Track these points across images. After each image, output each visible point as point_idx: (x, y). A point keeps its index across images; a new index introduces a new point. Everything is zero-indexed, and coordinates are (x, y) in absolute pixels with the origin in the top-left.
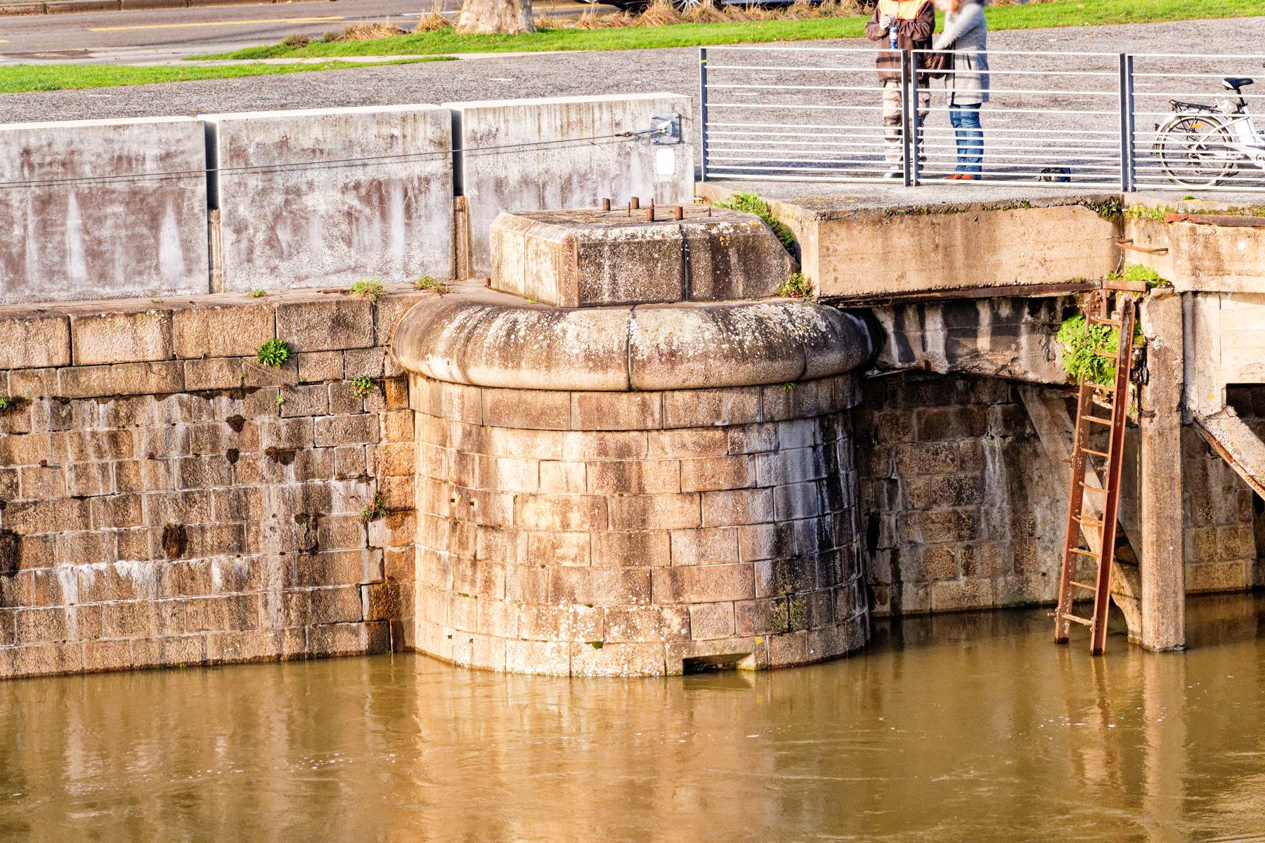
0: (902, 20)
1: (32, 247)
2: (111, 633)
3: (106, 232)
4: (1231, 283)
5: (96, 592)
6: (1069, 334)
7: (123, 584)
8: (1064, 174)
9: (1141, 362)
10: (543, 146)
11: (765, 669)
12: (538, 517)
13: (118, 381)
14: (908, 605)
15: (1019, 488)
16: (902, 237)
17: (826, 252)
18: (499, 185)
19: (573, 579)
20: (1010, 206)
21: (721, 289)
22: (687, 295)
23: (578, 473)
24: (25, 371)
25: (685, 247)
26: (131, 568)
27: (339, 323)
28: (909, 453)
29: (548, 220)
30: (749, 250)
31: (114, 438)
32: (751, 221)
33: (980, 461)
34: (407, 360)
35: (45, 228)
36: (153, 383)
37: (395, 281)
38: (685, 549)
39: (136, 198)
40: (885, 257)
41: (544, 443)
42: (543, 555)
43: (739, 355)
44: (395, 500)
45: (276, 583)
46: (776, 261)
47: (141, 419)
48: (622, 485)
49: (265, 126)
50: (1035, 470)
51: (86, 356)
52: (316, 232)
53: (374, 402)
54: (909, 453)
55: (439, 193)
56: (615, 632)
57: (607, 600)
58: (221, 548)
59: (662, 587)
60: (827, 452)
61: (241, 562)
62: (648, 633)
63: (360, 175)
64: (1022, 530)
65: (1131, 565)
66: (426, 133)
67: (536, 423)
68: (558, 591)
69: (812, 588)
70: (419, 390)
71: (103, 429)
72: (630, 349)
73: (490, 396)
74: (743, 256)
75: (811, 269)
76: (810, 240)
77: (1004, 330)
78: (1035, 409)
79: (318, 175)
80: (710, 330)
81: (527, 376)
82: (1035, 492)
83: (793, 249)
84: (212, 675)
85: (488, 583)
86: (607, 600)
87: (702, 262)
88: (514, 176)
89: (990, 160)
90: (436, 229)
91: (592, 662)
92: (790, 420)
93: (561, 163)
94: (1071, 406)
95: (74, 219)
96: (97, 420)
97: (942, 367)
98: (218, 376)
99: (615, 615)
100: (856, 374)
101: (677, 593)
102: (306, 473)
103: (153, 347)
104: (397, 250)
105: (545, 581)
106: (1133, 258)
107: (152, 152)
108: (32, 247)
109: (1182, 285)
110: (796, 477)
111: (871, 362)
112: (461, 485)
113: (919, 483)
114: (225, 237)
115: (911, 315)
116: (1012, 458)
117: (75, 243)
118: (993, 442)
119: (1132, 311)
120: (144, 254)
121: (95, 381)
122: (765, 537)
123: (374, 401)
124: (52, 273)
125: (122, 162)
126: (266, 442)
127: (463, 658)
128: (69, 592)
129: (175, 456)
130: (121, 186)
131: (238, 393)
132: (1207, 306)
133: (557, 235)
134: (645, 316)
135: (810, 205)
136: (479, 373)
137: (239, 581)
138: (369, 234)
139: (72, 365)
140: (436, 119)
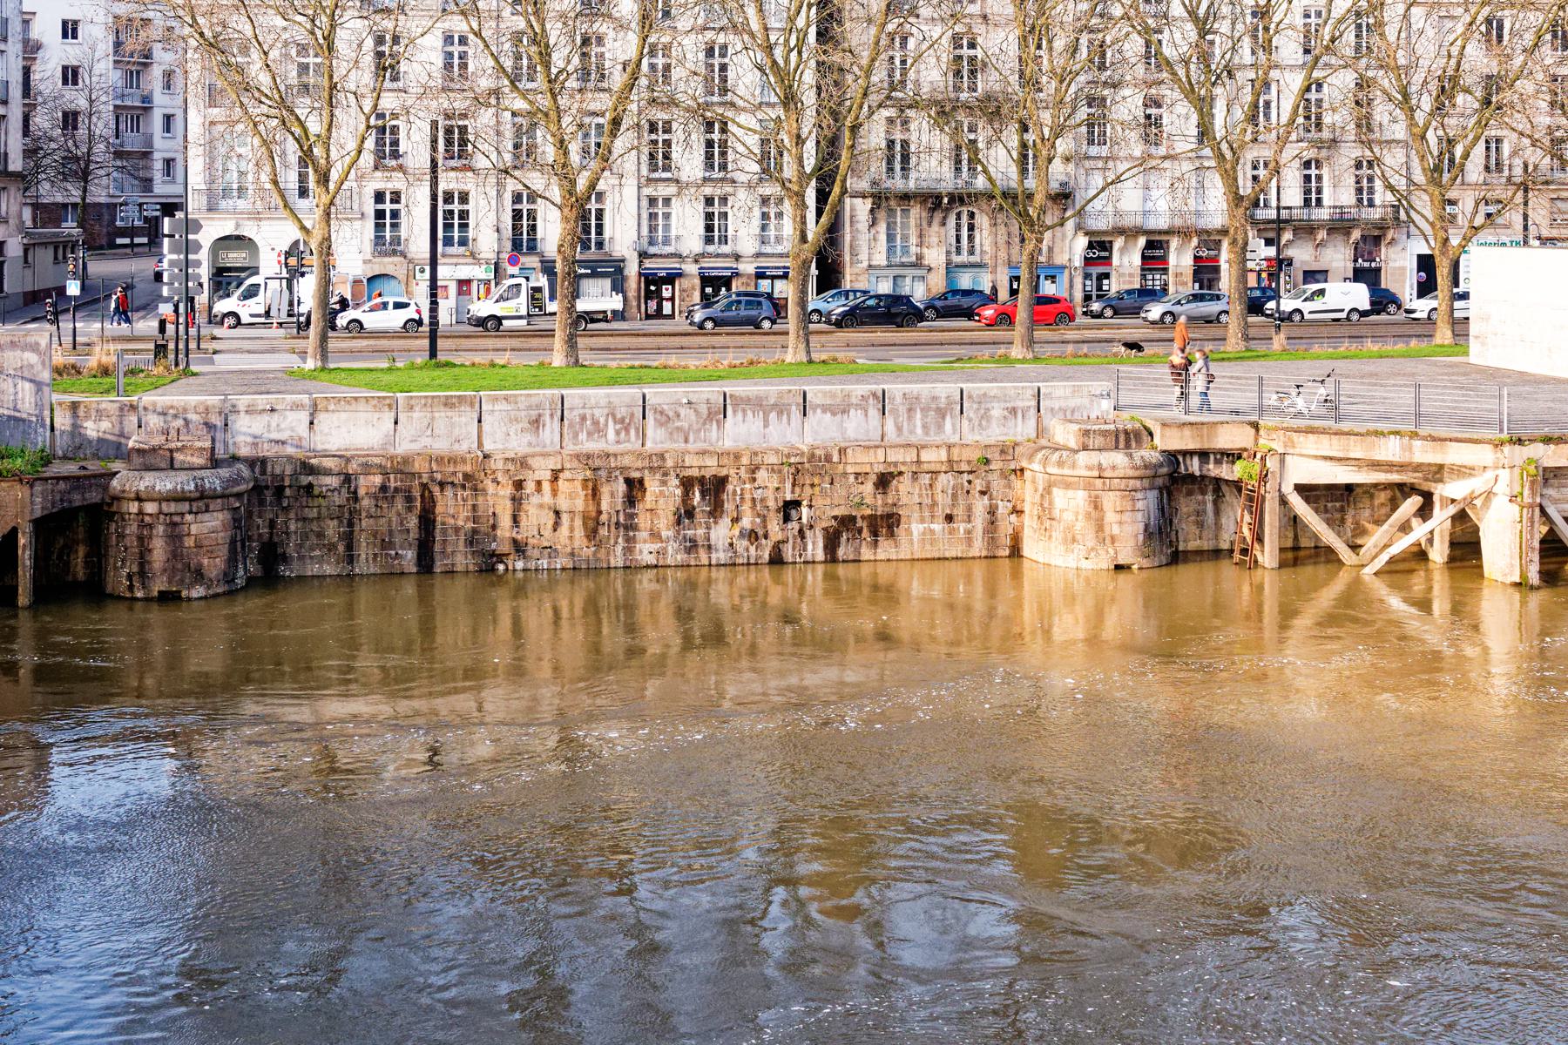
1: (905, 424)
2: (928, 547)
4: (1297, 451)
5: (924, 534)
6: (1239, 465)
7: (932, 532)
8: (1237, 413)
9: (1266, 475)
10: (1066, 398)
11: (1140, 569)
12: (1068, 517)
13: (933, 467)
14: (1181, 548)
15: (1217, 512)
16: (1187, 432)
17: (1162, 436)
18: (1052, 409)
19: (1078, 537)
20: (1222, 423)
21: (1128, 446)
22: (1117, 448)
23: (1082, 503)
24: (904, 463)
25: (1117, 433)
27: (1002, 452)
29: (1071, 421)
30: (1137, 435)
32: (1138, 425)
33: (1204, 503)
34: (1024, 464)
35: (910, 418)
36: (944, 468)
37: (1019, 439)
38: (1116, 530)
39: (938, 410)
40: (1182, 437)
41: (1070, 493)
42: (1069, 528)
43: (1136, 468)
44: (1018, 508)
45: (980, 533)
46: (1145, 437)
47: (940, 479)
48: (1096, 507)
49: (979, 388)
50: (1223, 507)
51: (923, 458)
52: (994, 423)
53: (1013, 477)
54: (1182, 500)
55: (1033, 411)
56: (1092, 554)
57: (1090, 544)
58: (964, 521)
59: (1108, 541)
61: (969, 526)
63: (1009, 405)
64: (1218, 526)
65: (1260, 540)
67: (1068, 486)
68: (1074, 540)
70: (1027, 474)
71: (927, 482)
72: (1100, 464)
73: (1053, 478)
74: (1135, 436)
75: (1157, 440)
76: (1157, 432)
77: (1218, 462)
78: (1224, 488)
79: (995, 405)
80: (1126, 459)
81: (1066, 471)
82: (1222, 514)
83: (1151, 434)
84: (959, 562)
85: (1050, 537)
86: (1090, 544)
88: (1057, 407)
89: (1213, 405)
90: (1032, 423)
91: (1085, 564)
93: (1072, 403)
94: (1240, 490)
95: (919, 415)
96: (925, 479)
97: (1197, 473)
98: (964, 467)
99: (1092, 549)
100: (1170, 475)
101: (1113, 543)
102: (991, 499)
103: (944, 457)
104: (1019, 429)
105: (1070, 536)
106: (1261, 441)
107: (944, 395)
108: (905, 424)
109: (1281, 451)
110: (1152, 506)
111: (1175, 472)
112: (1042, 505)
113: (1185, 510)
114: (965, 423)
115: (1188, 457)
116: (1215, 502)
117: (919, 423)
118: (1209, 498)
119: (1263, 459)
120: (940, 427)
121: (926, 467)
122: (1141, 527)
123: (1013, 477)
124: (912, 432)
125: (934, 398)
126: (979, 488)
127: (1041, 560)
128: (915, 534)
129: (950, 492)
130: (933, 406)
131: (970, 472)
133: (1076, 427)
134: (1105, 454)
135: (1156, 420)
136: (1050, 470)
137: (969, 532)
138: (1011, 423)
139: (918, 462)
140: (1033, 388)
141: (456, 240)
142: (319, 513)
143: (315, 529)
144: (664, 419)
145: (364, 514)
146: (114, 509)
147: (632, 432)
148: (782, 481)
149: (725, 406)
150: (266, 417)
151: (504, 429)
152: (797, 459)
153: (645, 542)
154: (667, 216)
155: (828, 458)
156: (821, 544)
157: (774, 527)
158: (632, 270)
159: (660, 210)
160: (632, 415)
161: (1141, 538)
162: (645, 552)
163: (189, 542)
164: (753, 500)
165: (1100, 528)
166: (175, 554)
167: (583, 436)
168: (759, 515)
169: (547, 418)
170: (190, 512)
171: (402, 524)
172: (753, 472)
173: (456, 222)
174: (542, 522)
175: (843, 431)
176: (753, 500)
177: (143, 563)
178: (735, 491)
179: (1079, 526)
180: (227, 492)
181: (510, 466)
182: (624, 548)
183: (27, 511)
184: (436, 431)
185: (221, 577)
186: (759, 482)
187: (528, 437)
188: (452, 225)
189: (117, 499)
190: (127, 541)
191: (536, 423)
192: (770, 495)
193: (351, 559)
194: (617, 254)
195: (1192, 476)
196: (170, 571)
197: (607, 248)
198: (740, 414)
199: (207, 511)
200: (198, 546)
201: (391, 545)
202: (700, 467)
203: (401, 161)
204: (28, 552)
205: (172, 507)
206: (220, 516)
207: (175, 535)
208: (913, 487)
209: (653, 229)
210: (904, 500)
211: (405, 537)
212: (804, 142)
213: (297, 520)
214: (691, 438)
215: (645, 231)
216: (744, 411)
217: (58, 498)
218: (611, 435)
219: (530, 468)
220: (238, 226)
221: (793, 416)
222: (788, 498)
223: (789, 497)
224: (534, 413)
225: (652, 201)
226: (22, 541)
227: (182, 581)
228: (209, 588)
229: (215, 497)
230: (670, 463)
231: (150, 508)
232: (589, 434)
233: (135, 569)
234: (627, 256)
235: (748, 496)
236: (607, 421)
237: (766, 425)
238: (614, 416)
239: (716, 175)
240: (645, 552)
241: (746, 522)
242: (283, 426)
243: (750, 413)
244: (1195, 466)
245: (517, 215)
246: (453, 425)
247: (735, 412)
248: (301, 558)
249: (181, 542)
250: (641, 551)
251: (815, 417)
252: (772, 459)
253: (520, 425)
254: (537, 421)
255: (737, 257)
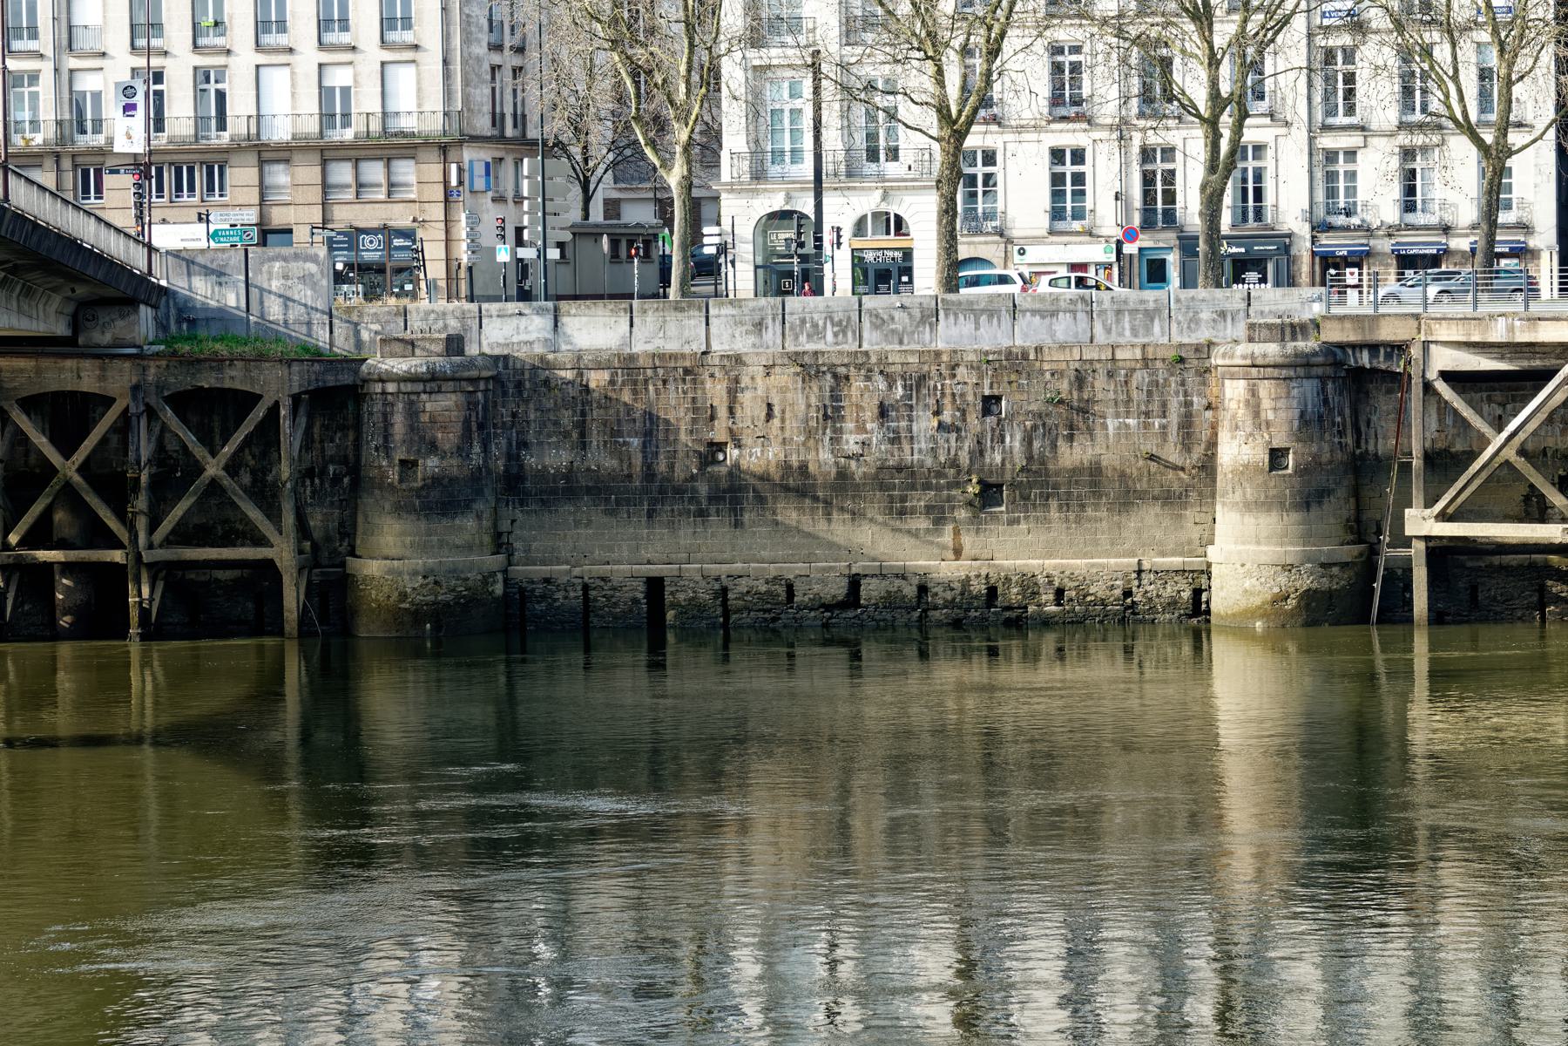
0: (1536, 284)
3: (1137, 323)
5: (1119, 428)
7: (1128, 426)
25: (1282, 327)
26: (1131, 422)
28: (1381, 398)
31: (1126, 382)
35: (1118, 321)
38: (1271, 415)
40: (1342, 330)
42: (1234, 416)
48: (1253, 395)
52: (1203, 324)
54: (1381, 398)
58: (1159, 417)
60: (1324, 389)
61: (1164, 421)
62: (1260, 440)
66: (1238, 296)
68: (1237, 427)
69: (1315, 429)
77: (1389, 356)
86: (1248, 430)
87: (1288, 331)
92: (1308, 378)
95: (1127, 318)
97: (1368, 366)
99: (1251, 435)
104: (1229, 331)
110: (1309, 396)
113: (1385, 408)
115: (1357, 350)
117: (1127, 326)
122: (1297, 413)
124: (1121, 334)
128: (1111, 428)
132: (1432, 347)
137: (1164, 427)
138: (1221, 326)
139: (1113, 359)
141: (1069, 211)
142: (555, 404)
143: (552, 418)
144: (879, 322)
145: (595, 405)
146: (365, 391)
147: (850, 334)
148: (981, 377)
149: (937, 310)
150: (515, 320)
151: (730, 331)
152: (996, 357)
153: (851, 433)
154: (1351, 176)
155: (1025, 356)
156: (1018, 437)
157: (973, 420)
158: (1303, 249)
159: (1341, 167)
160: (849, 318)
161: (1296, 423)
162: (852, 442)
163: (425, 418)
164: (953, 395)
165: (1256, 414)
166: (413, 427)
167: (803, 338)
168: (959, 409)
169: (770, 321)
170: (425, 392)
171: (629, 415)
172: (953, 369)
173: (1069, 188)
174: (756, 413)
175: (1052, 334)
176: (953, 395)
177: (387, 437)
178: (935, 387)
179: (1241, 412)
180: (457, 375)
181: (726, 362)
182: (831, 439)
183: (286, 388)
184: (669, 333)
185: (454, 450)
186: (959, 378)
187: (752, 339)
188: (1064, 192)
189: (365, 381)
190: (375, 418)
191: (759, 326)
192: (969, 389)
193: (584, 446)
194: (1284, 229)
195: (1363, 368)
196: (408, 442)
197: (1269, 217)
198: (952, 318)
199: (439, 392)
200: (433, 421)
201: (619, 433)
202: (902, 364)
203: (995, 110)
204: (287, 422)
205: (409, 387)
206: (453, 397)
207: (413, 412)
208: (1109, 384)
209: (1331, 193)
210: (1099, 396)
211: (632, 425)
212: (1219, 63)
213: (536, 410)
214: (906, 341)
215: (1320, 196)
216: (956, 315)
217: (313, 377)
218: (830, 336)
219: (744, 364)
220: (788, 198)
221: (1003, 319)
222: (987, 393)
223: (987, 392)
224: (757, 318)
225: (1331, 156)
226: (283, 412)
227: (419, 451)
228: (443, 458)
229: (447, 380)
230: (874, 359)
231: (391, 388)
232: (809, 336)
233: (381, 442)
234: (1296, 230)
235: (948, 391)
236: (825, 323)
237: (977, 328)
238: (832, 319)
239: (1418, 116)
240: (852, 442)
241: (947, 416)
242: (530, 328)
243: (961, 317)
244: (1365, 359)
245: (1148, 180)
246: (682, 327)
247: (947, 316)
248: (540, 444)
249: (417, 417)
250: (847, 442)
251: (1023, 322)
252: (972, 357)
253: (745, 328)
254: (760, 324)
255: (1446, 229)
